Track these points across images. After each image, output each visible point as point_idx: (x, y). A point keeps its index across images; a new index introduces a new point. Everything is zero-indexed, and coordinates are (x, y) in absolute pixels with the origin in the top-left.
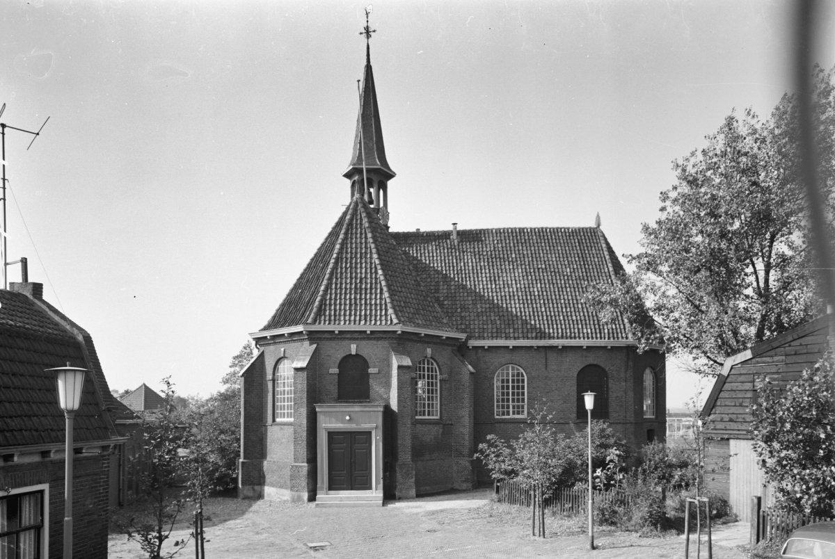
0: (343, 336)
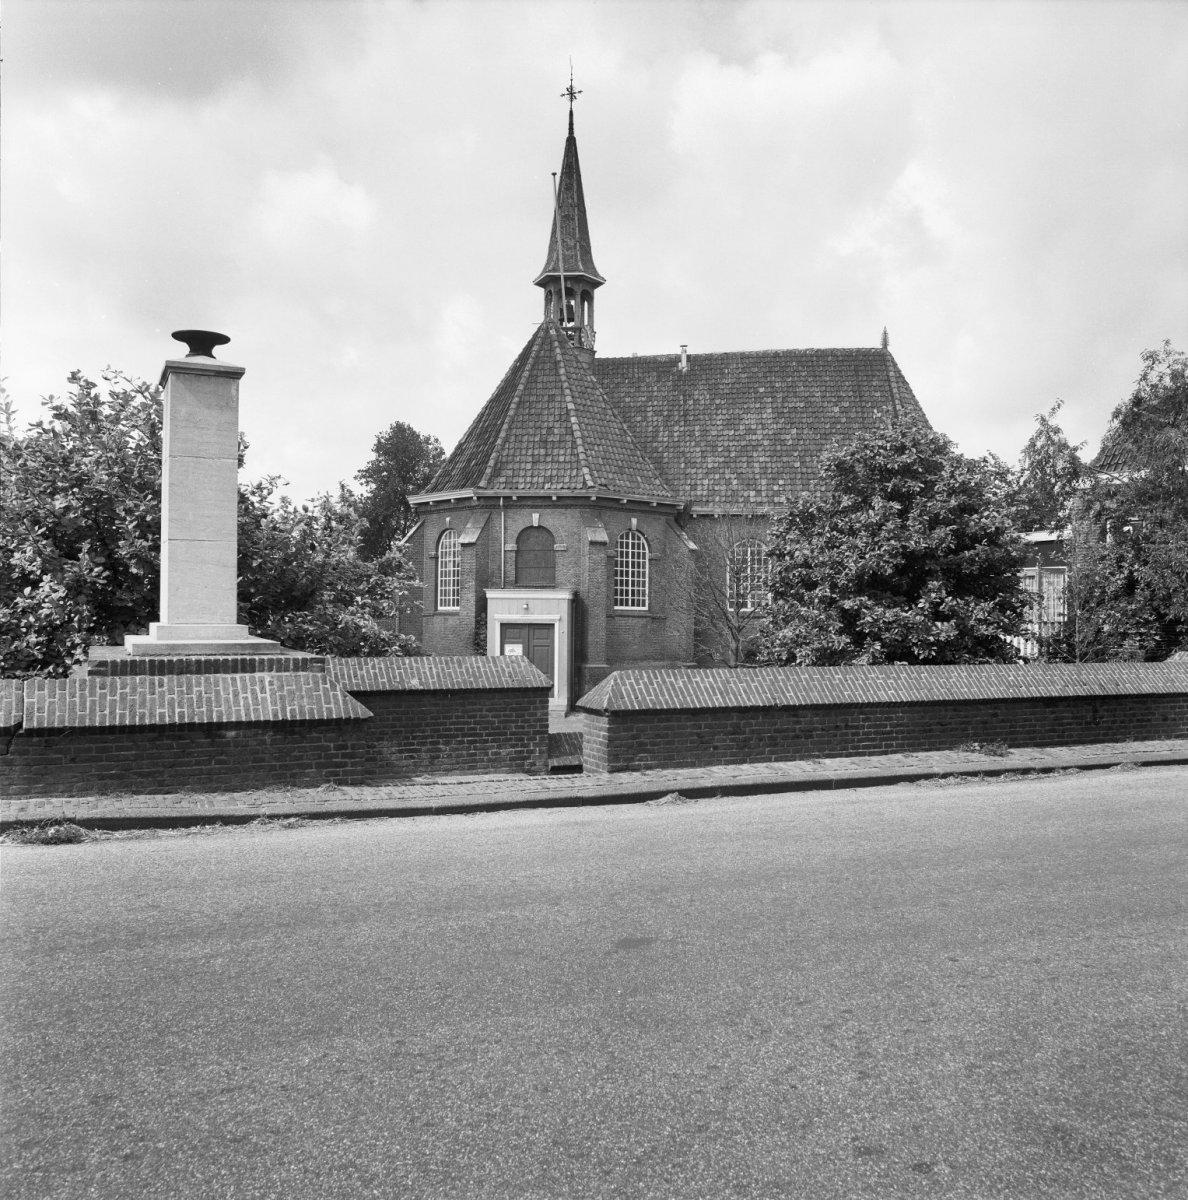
0: (523, 503)
